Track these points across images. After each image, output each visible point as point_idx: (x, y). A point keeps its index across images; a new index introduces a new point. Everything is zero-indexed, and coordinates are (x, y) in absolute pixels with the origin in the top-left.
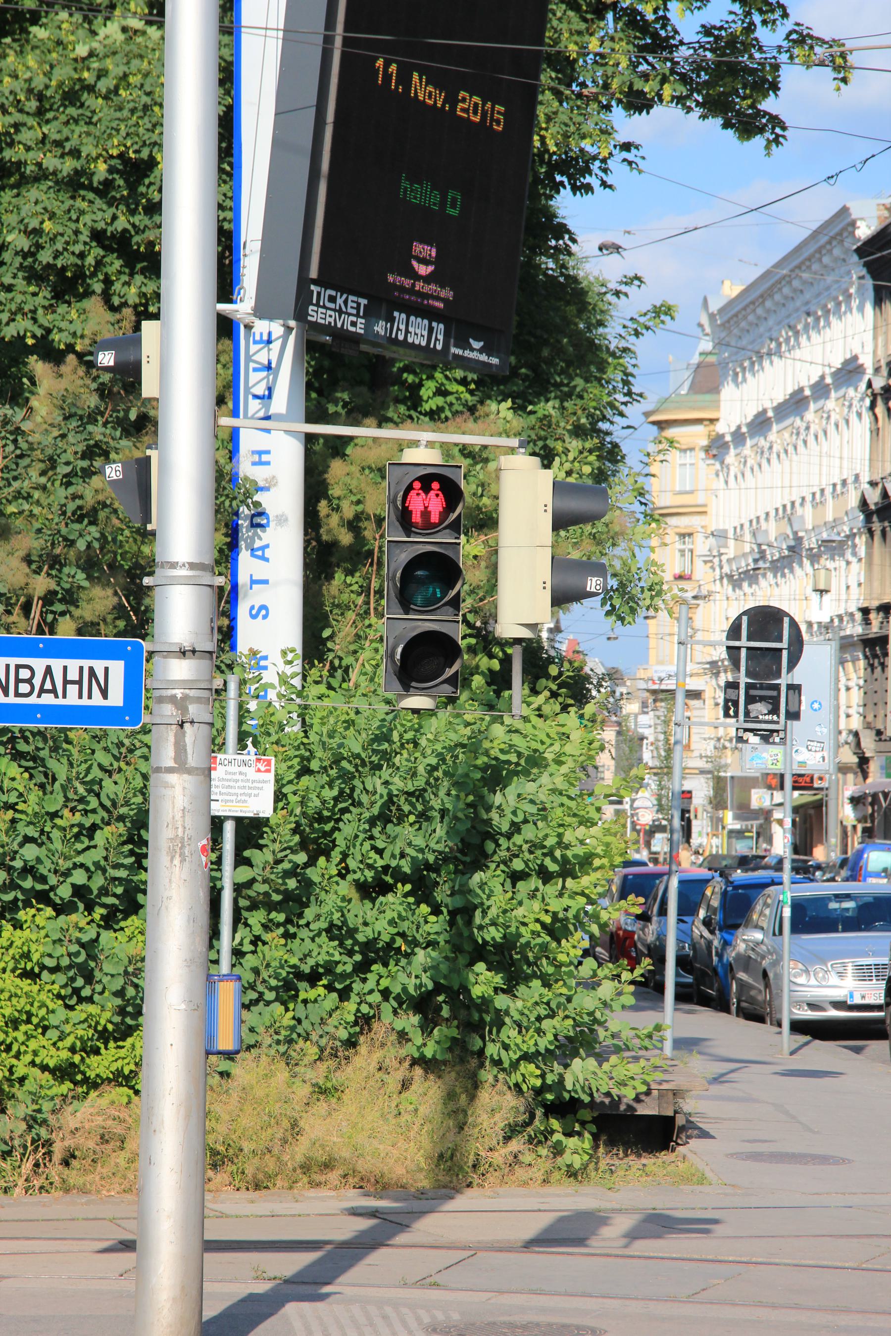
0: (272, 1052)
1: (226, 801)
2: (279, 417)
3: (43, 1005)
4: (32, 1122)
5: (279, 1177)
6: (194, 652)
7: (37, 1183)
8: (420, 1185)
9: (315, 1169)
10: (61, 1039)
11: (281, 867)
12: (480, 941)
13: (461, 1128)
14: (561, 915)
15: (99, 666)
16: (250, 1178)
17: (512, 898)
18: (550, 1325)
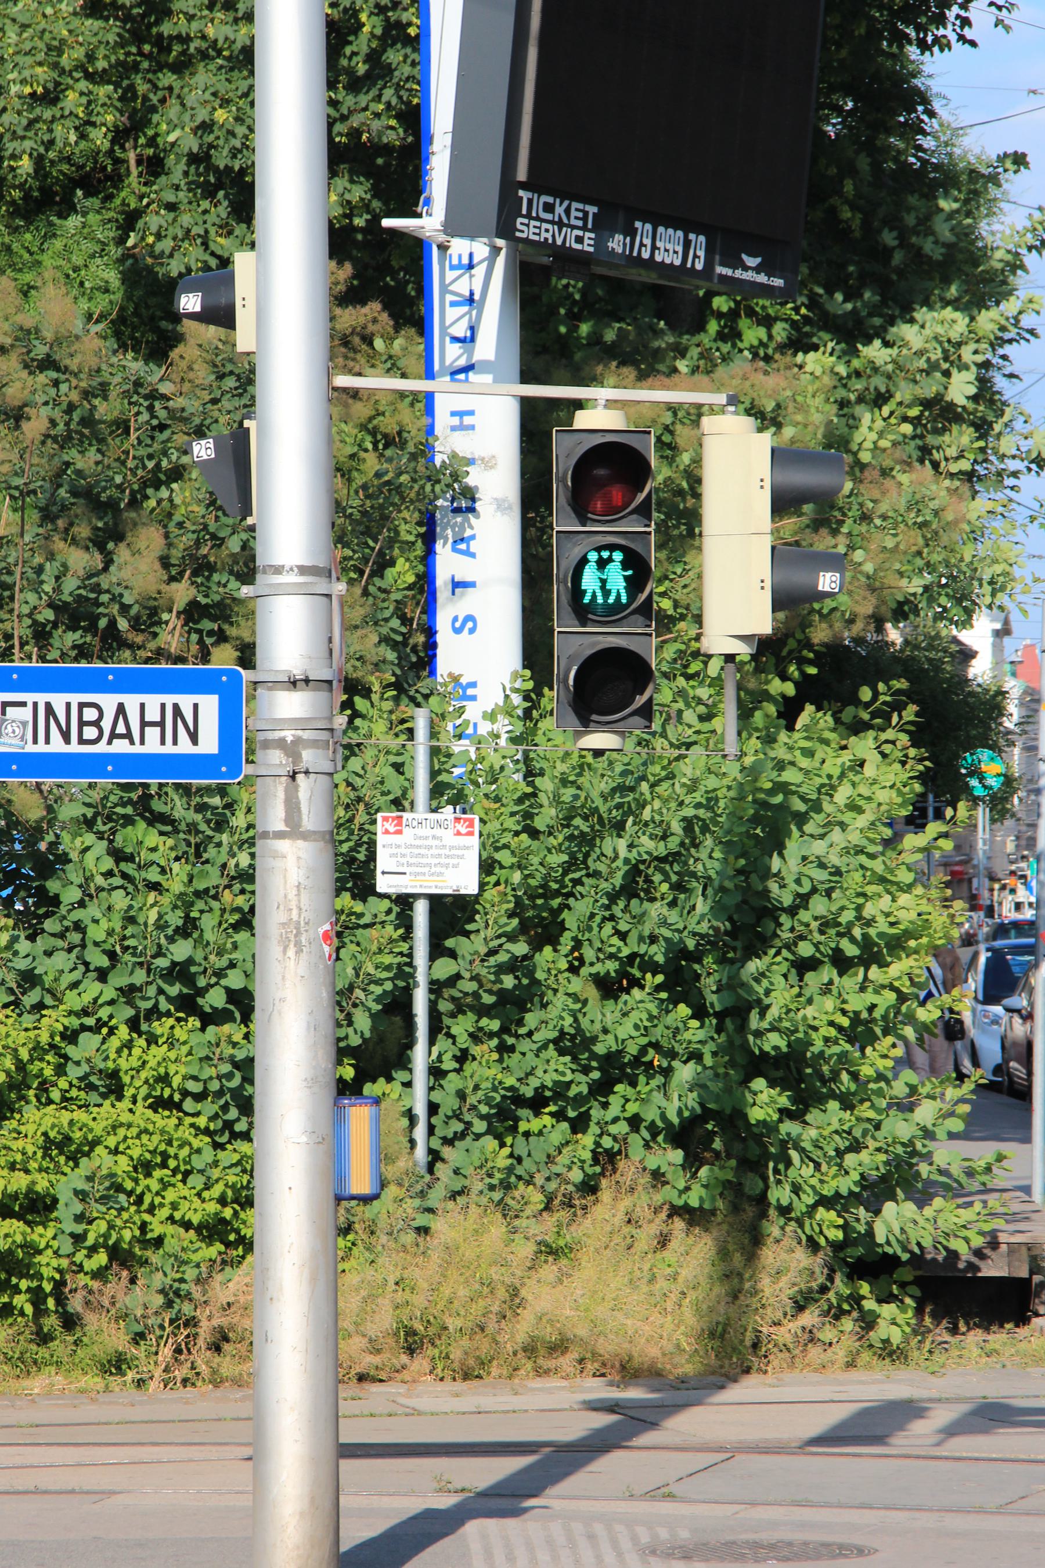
0: (484, 1200)
1: (417, 874)
2: (485, 367)
3: (184, 1143)
4: (172, 1296)
5: (495, 1363)
6: (307, 681)
7: (179, 1374)
8: (680, 1371)
9: (542, 1352)
10: (207, 1187)
11: (492, 961)
12: (757, 1052)
13: (735, 1295)
14: (865, 1015)
15: (186, 702)
16: (456, 1366)
17: (800, 995)
18: (806, 1544)
